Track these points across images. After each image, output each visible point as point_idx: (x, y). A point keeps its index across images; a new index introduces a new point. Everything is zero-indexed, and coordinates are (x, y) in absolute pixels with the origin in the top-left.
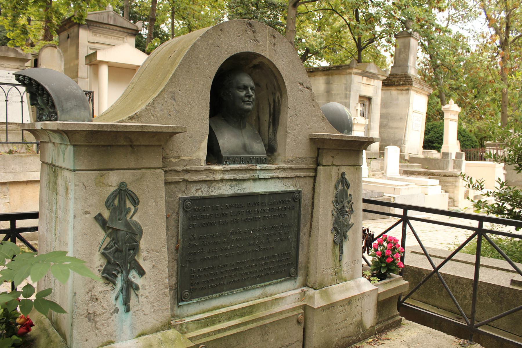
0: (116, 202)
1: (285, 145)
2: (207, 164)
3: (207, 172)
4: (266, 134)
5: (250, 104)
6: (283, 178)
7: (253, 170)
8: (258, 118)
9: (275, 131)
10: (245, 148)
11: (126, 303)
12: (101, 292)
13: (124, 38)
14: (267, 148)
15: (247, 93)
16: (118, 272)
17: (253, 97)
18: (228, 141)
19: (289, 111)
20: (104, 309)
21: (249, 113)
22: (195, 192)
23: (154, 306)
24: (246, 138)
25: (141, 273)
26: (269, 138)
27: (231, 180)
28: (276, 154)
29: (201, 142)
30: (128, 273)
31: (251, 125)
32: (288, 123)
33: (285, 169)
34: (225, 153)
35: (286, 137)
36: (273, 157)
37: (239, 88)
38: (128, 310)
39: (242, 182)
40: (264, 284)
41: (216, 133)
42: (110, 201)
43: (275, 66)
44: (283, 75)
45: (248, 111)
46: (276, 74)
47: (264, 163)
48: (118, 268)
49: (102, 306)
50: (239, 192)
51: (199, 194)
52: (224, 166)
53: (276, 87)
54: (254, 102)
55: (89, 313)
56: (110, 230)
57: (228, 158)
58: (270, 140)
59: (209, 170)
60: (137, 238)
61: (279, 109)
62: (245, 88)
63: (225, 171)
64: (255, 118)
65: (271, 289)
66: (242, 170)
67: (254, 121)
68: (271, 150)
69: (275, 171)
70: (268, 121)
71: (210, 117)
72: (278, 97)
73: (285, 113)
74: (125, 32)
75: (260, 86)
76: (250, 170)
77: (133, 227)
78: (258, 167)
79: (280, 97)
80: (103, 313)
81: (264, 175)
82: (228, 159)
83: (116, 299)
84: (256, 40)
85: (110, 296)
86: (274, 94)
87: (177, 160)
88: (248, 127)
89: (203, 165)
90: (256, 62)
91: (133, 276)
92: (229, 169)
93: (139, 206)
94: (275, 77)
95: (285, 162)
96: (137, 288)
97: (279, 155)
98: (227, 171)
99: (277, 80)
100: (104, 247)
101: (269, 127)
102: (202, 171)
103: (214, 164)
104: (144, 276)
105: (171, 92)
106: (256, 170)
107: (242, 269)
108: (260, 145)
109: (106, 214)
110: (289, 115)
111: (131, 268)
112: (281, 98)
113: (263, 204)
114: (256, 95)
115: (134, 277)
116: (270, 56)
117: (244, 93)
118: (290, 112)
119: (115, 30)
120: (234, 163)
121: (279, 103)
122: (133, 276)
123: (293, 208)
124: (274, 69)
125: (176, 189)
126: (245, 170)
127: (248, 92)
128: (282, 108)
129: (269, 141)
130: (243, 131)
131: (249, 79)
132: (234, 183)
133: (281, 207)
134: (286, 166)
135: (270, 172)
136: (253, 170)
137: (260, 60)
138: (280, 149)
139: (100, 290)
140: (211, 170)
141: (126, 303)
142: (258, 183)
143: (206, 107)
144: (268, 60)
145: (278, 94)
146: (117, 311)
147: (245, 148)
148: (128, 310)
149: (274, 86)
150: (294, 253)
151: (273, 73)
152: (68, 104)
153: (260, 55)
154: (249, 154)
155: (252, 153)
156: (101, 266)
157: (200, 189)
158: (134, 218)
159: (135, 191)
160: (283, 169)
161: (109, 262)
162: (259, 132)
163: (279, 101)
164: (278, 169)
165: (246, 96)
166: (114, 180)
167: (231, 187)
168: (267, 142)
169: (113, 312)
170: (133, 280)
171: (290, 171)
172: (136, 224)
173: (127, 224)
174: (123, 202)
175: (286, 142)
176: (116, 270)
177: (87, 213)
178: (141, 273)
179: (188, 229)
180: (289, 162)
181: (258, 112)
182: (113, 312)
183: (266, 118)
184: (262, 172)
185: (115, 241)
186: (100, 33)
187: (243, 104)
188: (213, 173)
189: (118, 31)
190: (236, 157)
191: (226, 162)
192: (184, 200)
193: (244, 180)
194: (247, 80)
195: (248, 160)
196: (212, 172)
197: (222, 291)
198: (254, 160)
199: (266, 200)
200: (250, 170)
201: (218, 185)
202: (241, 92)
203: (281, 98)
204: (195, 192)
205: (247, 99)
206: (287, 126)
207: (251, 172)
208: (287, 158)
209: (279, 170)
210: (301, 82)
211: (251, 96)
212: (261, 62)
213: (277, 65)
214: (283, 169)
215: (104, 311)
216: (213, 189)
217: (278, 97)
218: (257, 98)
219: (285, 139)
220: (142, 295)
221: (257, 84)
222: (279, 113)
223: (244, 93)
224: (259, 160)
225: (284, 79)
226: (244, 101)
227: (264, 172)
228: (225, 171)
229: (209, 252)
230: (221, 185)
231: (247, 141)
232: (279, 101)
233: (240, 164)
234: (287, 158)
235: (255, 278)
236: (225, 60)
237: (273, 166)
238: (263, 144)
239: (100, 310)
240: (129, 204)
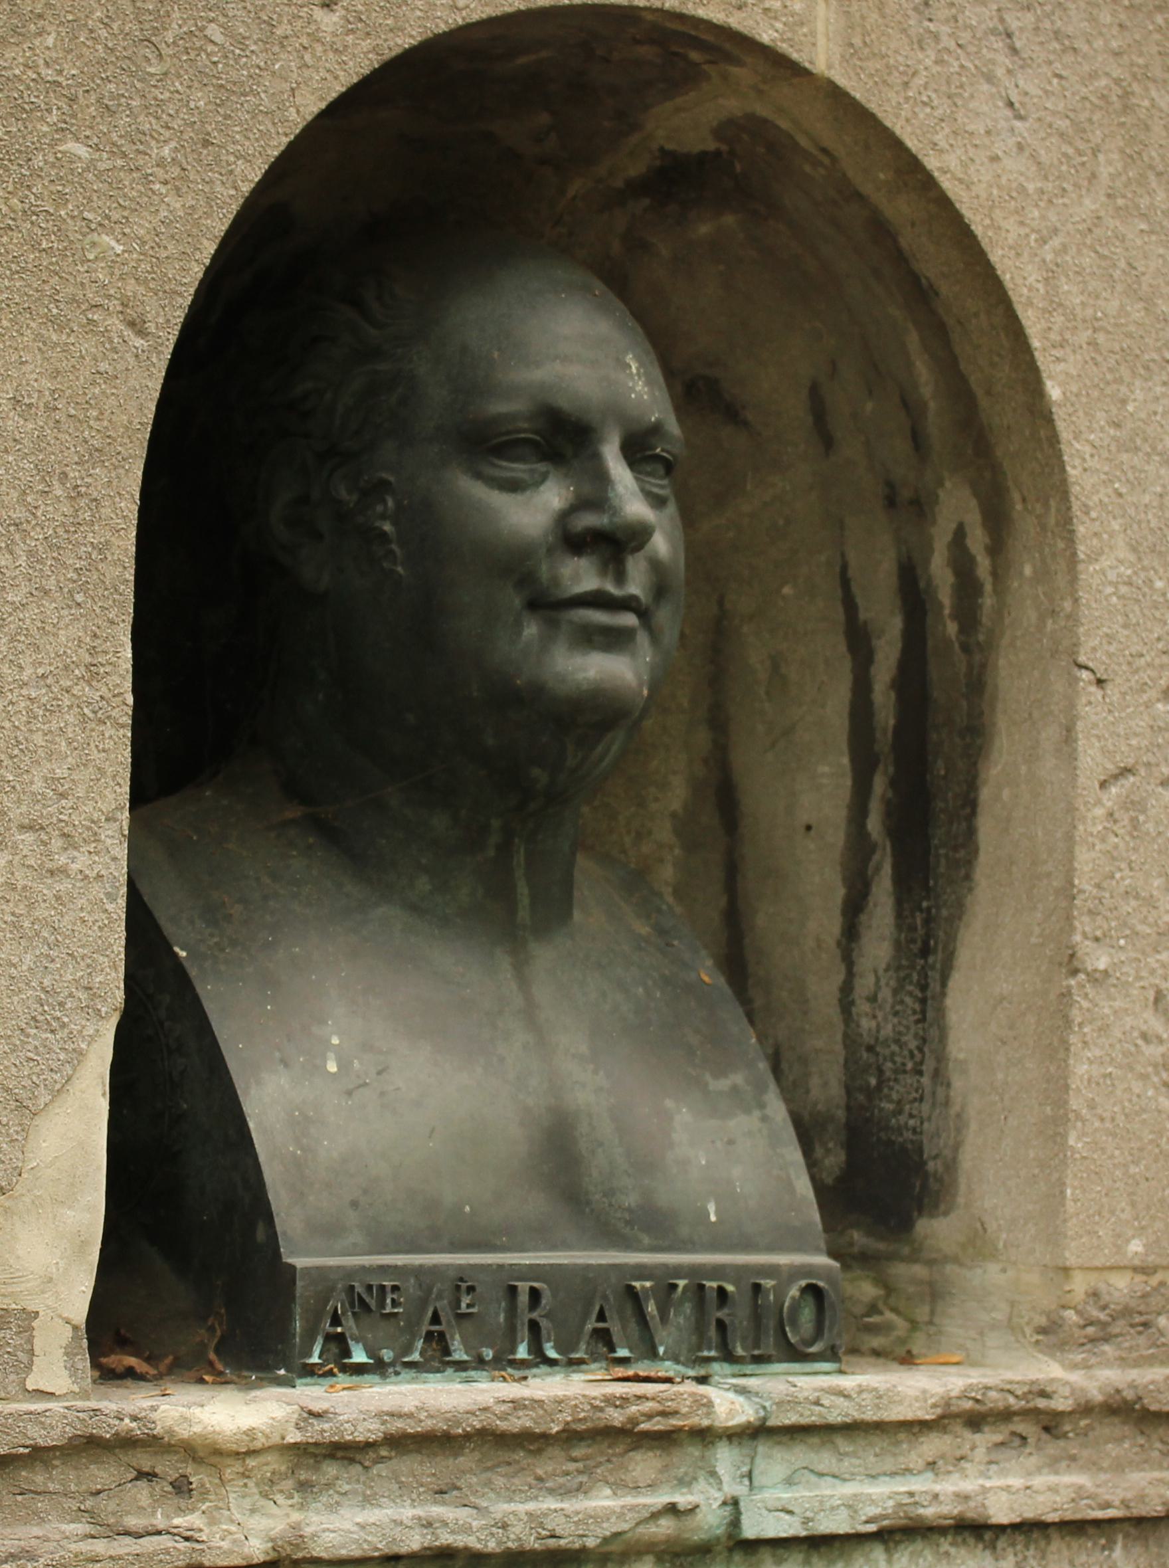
1: (1056, 1124)
2: (108, 1375)
3: (102, 1474)
4: (823, 989)
5: (614, 640)
6: (1030, 1530)
7: (665, 1440)
8: (723, 798)
9: (926, 954)
10: (560, 1162)
14: (834, 1160)
15: (581, 505)
17: (660, 544)
18: (369, 1078)
19: (1092, 708)
21: (615, 742)
24: (571, 1041)
26: (851, 1041)
28: (939, 1231)
29: (27, 1110)
31: (636, 882)
32: (1085, 859)
33: (1051, 1424)
34: (327, 1231)
35: (1059, 1017)
36: (905, 1272)
37: (488, 445)
41: (209, 992)
43: (913, 174)
44: (1021, 276)
45: (600, 714)
46: (932, 261)
47: (795, 1355)
52: (311, 1394)
53: (936, 421)
54: (664, 616)
57: (365, 1299)
58: (865, 1067)
59: (126, 1443)
61: (977, 685)
62: (562, 438)
63: (322, 1457)
64: (677, 796)
66: (531, 1442)
67: (664, 832)
68: (881, 1181)
69: (932, 1445)
70: (837, 837)
71: (139, 797)
72: (960, 534)
73: (1050, 734)
75: (732, 414)
76: (631, 1437)
78: (728, 1400)
79: (977, 541)
81: (801, 1495)
82: (360, 1307)
86: (908, 506)
88: (595, 908)
89: (57, 1384)
90: (684, 124)
92: (370, 1430)
94: (919, 294)
95: (1050, 1334)
97: (979, 1245)
98: (345, 1452)
99: (938, 332)
101: (855, 906)
102: (39, 1455)
103: (191, 1366)
106: (705, 1436)
108: (742, 1123)
110: (1091, 758)
112: (996, 549)
114: (688, 518)
116: (851, 54)
117: (553, 496)
118: (1106, 728)
120: (439, 1358)
121: (968, 615)
124: (900, 210)
126: (571, 1437)
127: (596, 493)
128: (1012, 679)
129: (853, 1069)
130: (544, 955)
131: (603, 327)
134: (1068, 1378)
135: (868, 1454)
136: (665, 1440)
137: (732, 105)
138: (990, 1176)
140: (154, 1443)
143: (93, 674)
144: (836, 95)
145: (956, 506)
147: (560, 1162)
149: (911, 407)
151: (900, 259)
153: (730, 46)
154: (608, 1233)
155: (656, 1225)
160: (1037, 1423)
162: (737, 965)
163: (967, 586)
164: (975, 1421)
165: (574, 542)
168: (827, 1088)
171: (1119, 1443)
175: (1057, 1087)
179: (944, 1048)
180: (1102, 1328)
181: (718, 722)
183: (810, 797)
184: (774, 1463)
187: (531, 630)
188: (182, 1487)
190: (462, 1283)
191: (339, 1345)
194: (575, 348)
195: (605, 1321)
196: (168, 1467)
198: (682, 1317)
200: (631, 1437)
202: (513, 486)
203: (996, 549)
205: (582, 576)
206: (1068, 892)
207: (644, 1464)
208: (1079, 1285)
209: (989, 1436)
211: (638, 535)
212: (755, 127)
213: (945, 163)
214: (1037, 1423)
217: (960, 534)
218: (702, 555)
219: (1056, 1051)
221: (695, 390)
222: (975, 736)
223: (553, 496)
224: (739, 1316)
225: (1031, 321)
226: (547, 604)
227: (800, 1455)
228: (322, 1457)
231: (592, 1081)
232: (967, 586)
233: (504, 1363)
234: (1079, 1285)
236: (311, 105)
237: (913, 1389)
238: (778, 1109)
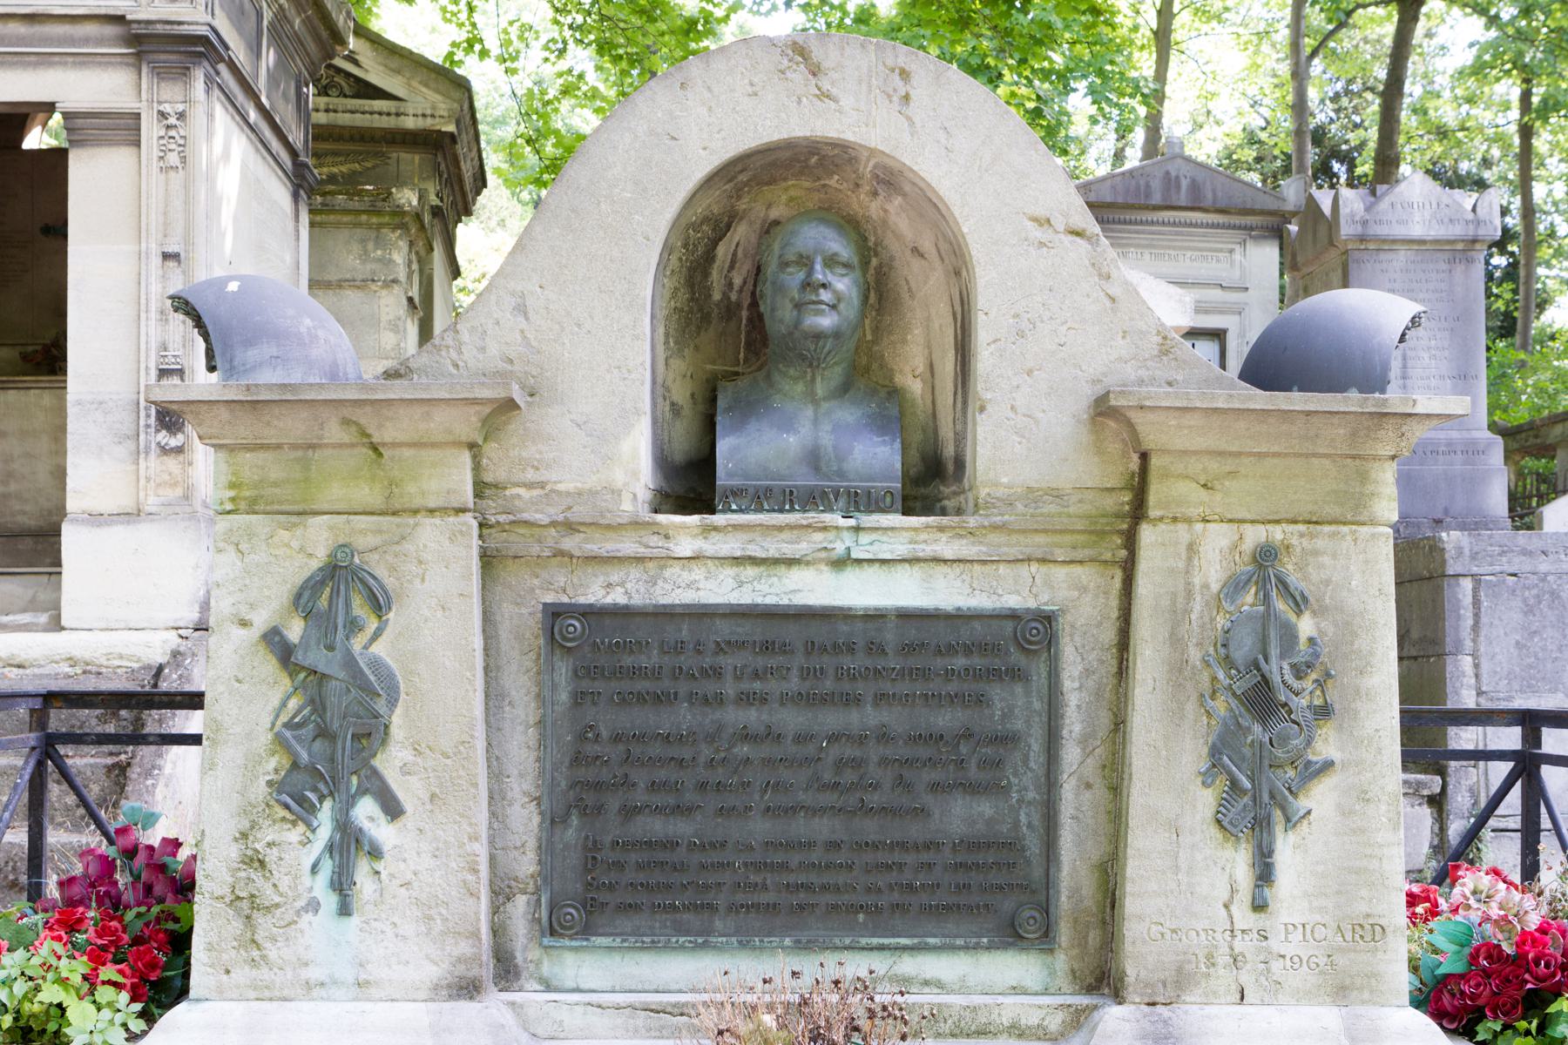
0: (323, 602)
10: (814, 458)
11: (342, 885)
12: (269, 845)
13: (1231, 251)
16: (322, 798)
20: (281, 895)
22: (597, 591)
23: (430, 918)
25: (393, 810)
27: (737, 561)
30: (351, 802)
38: (345, 910)
39: (782, 569)
40: (886, 941)
42: (306, 595)
48: (321, 786)
49: (275, 885)
50: (769, 600)
51: (617, 597)
55: (238, 898)
56: (302, 675)
57: (737, 493)
60: (381, 706)
65: (909, 965)
74: (1234, 227)
77: (366, 669)
80: (277, 906)
83: (314, 869)
84: (824, 95)
85: (300, 851)
87: (536, 492)
91: (366, 811)
93: (391, 615)
96: (375, 853)
100: (284, 718)
104: (403, 819)
105: (513, 294)
107: (784, 867)
109: (295, 631)
111: (362, 791)
113: (876, 648)
115: (371, 819)
119: (1196, 225)
122: (366, 811)
123: (1017, 675)
125: (536, 582)
132: (750, 571)
133: (960, 662)
139: (269, 839)
141: (342, 885)
142: (851, 575)
146: (314, 906)
148: (345, 910)
150: (1033, 845)
152: (250, 353)
155: (841, 474)
156: (276, 771)
157: (622, 584)
158: (378, 649)
159: (381, 572)
161: (295, 765)
166: (316, 542)
167: (741, 584)
169: (305, 909)
170: (366, 825)
172: (376, 664)
173: (350, 662)
174: (341, 600)
176: (315, 789)
177: (244, 623)
178: (393, 810)
182: (305, 909)
185: (317, 704)
186: (1137, 246)
189: (1208, 226)
192: (555, 614)
193: (791, 562)
197: (707, 932)
199: (890, 637)
201: (685, 574)
204: (603, 592)
210: (1041, 212)
215: (277, 899)
216: (667, 586)
220: (392, 876)
229: (653, 787)
230: (697, 573)
235: (855, 909)
239: (269, 895)
240: (360, 608)
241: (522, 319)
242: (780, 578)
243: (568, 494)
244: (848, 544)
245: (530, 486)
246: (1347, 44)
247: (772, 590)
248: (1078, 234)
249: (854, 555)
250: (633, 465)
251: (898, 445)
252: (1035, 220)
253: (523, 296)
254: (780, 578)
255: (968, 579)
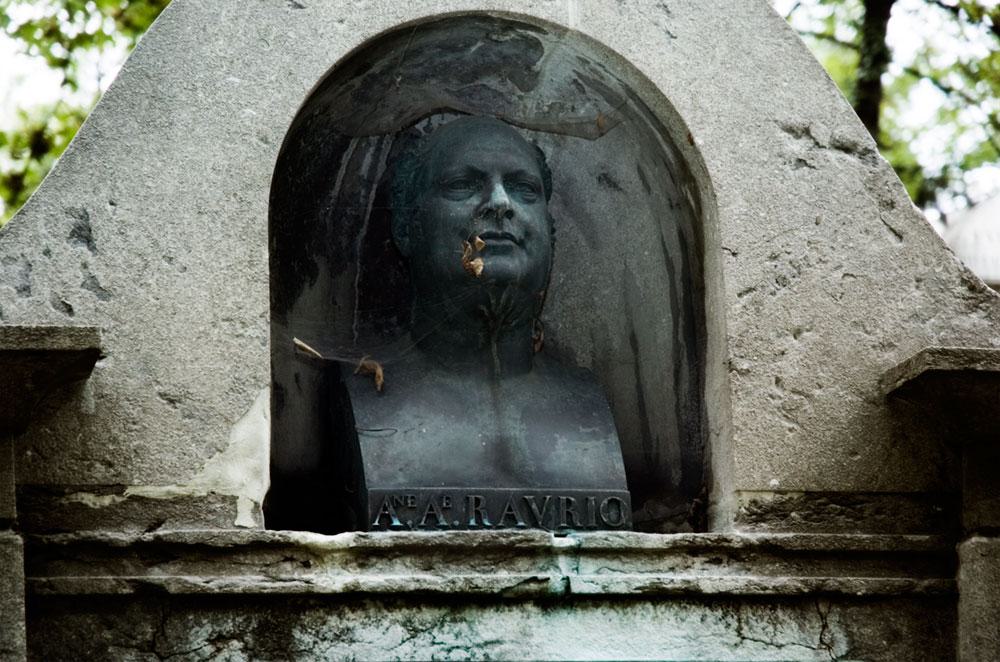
10: (501, 455)
125: (108, 635)
210: (797, 120)
241: (84, 248)
242: (470, 624)
243: (158, 502)
244: (565, 573)
245: (100, 490)
246: (814, 485)
247: (459, 642)
248: (847, 148)
249: (576, 588)
250: (239, 466)
251: (614, 439)
252: (790, 130)
253: (85, 216)
254: (470, 624)
255: (735, 624)
